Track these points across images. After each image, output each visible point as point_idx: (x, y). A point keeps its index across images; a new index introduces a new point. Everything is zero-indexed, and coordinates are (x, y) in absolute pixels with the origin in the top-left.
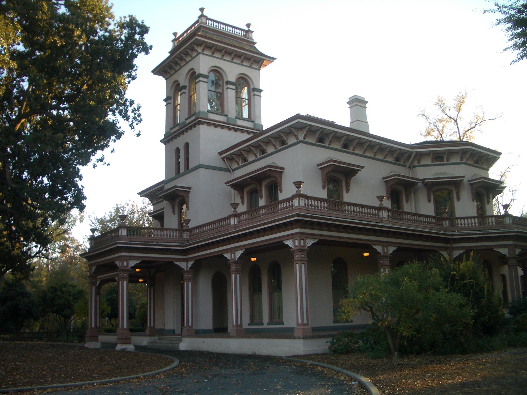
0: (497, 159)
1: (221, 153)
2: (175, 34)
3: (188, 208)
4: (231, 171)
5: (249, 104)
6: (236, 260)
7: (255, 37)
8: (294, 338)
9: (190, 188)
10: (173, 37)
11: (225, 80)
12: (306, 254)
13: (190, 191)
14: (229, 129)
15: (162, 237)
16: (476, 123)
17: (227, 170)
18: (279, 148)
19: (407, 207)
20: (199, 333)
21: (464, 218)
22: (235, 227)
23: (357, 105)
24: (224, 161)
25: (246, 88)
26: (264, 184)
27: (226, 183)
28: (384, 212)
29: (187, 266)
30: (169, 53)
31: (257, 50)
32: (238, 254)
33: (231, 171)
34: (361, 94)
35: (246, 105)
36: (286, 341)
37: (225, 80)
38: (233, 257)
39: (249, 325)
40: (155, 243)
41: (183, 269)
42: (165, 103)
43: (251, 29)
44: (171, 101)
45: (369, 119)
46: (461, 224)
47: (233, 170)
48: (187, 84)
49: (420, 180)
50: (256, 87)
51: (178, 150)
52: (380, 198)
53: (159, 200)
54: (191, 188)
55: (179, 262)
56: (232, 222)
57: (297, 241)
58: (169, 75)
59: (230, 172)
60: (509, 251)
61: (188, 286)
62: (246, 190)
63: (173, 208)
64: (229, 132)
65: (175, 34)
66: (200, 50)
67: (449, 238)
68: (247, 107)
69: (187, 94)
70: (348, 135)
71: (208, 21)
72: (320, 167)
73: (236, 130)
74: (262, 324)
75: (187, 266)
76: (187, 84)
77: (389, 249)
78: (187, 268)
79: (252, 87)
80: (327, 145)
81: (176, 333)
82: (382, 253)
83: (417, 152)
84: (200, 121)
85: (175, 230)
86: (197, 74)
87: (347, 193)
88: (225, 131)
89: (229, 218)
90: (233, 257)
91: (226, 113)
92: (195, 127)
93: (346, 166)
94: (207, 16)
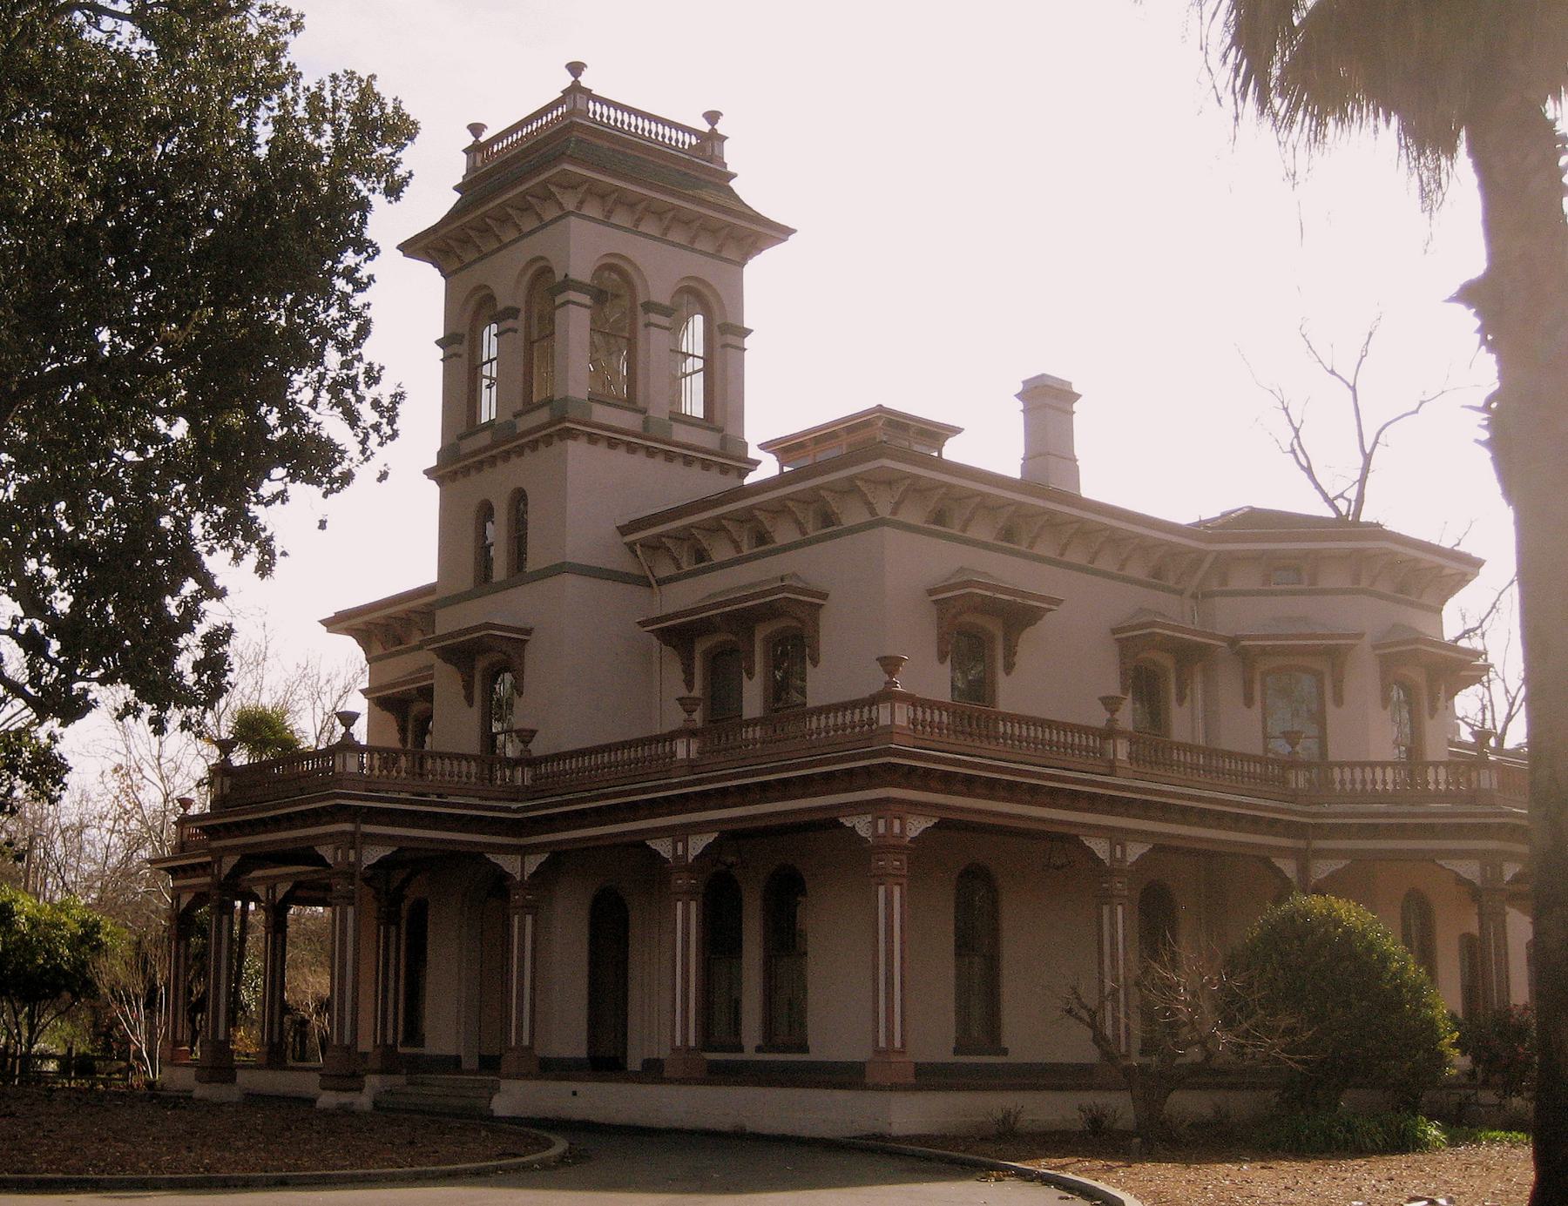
0: (1468, 578)
1: (624, 530)
2: (476, 129)
3: (518, 688)
4: (655, 585)
5: (708, 371)
6: (690, 861)
7: (733, 156)
8: (865, 1087)
9: (528, 632)
10: (469, 140)
11: (641, 299)
12: (904, 858)
13: (526, 641)
14: (651, 453)
15: (456, 779)
16: (1423, 398)
17: (643, 581)
18: (812, 534)
19: (1183, 724)
20: (552, 1069)
21: (1352, 765)
22: (692, 766)
23: (568, 302)
24: (634, 552)
25: (699, 320)
26: (762, 632)
27: (642, 624)
28: (1121, 744)
29: (523, 868)
30: (456, 188)
31: (737, 197)
32: (698, 844)
33: (655, 585)
34: (1058, 370)
35: (699, 371)
36: (840, 1095)
37: (641, 299)
38: (680, 852)
39: (759, 1049)
40: (434, 798)
41: (508, 876)
42: (440, 353)
43: (721, 128)
44: (463, 349)
45: (1080, 449)
46: (1342, 782)
47: (661, 582)
48: (520, 304)
49: (1223, 639)
50: (731, 320)
51: (486, 512)
52: (1110, 703)
53: (393, 649)
54: (532, 629)
55: (500, 857)
56: (681, 752)
57: (881, 823)
58: (457, 265)
59: (650, 586)
60: (1483, 869)
61: (522, 927)
62: (701, 647)
63: (468, 687)
64: (650, 461)
65: (476, 129)
66: (569, 202)
67: (1303, 824)
68: (698, 380)
69: (521, 335)
70: (1021, 504)
71: (591, 104)
72: (934, 598)
73: (669, 457)
74: (740, 1049)
75: (523, 868)
76: (520, 304)
77: (1128, 850)
78: (523, 875)
79: (718, 321)
80: (956, 531)
81: (465, 1066)
82: (1107, 862)
83: (1219, 553)
84: (569, 430)
85: (474, 758)
86: (559, 277)
87: (1008, 674)
88: (639, 459)
89: (672, 737)
90: (680, 852)
91: (640, 403)
92: (549, 444)
93: (1012, 598)
94: (591, 90)
